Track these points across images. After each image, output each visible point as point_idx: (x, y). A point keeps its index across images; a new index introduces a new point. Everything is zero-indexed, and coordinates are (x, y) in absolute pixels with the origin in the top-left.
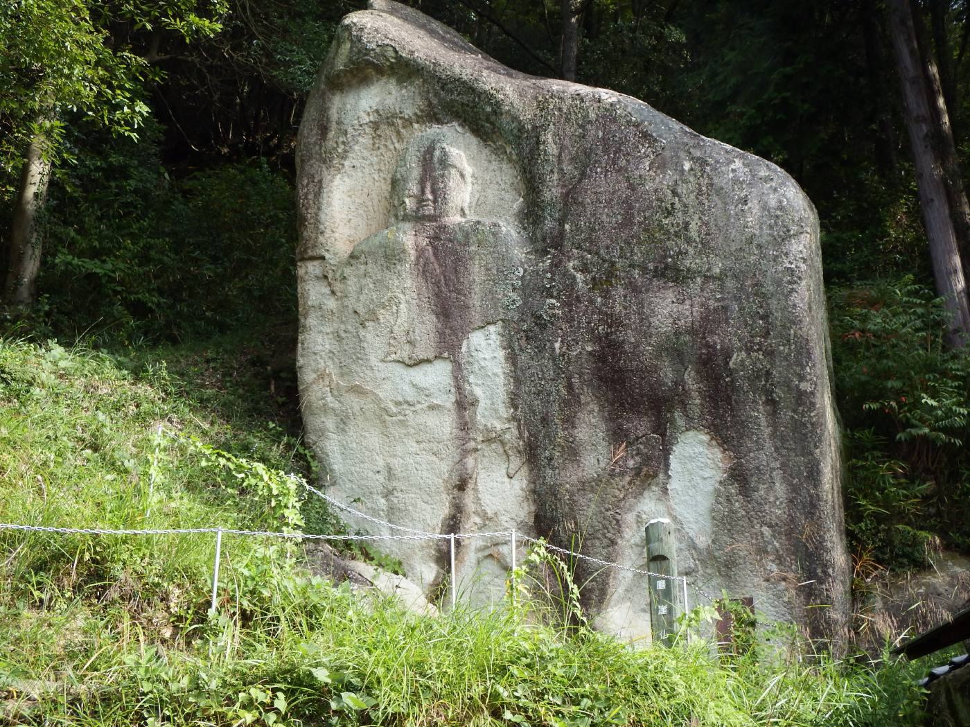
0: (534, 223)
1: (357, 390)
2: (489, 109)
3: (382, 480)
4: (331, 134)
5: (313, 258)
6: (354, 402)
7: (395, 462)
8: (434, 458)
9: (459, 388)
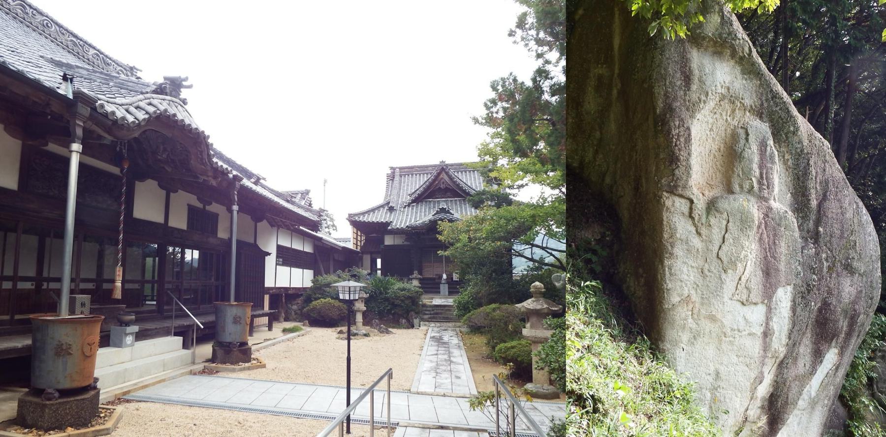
0: (803, 218)
1: (712, 318)
2: (792, 129)
3: (711, 380)
4: (694, 87)
5: (681, 196)
6: (707, 326)
7: (722, 369)
8: (747, 369)
9: (767, 324)
